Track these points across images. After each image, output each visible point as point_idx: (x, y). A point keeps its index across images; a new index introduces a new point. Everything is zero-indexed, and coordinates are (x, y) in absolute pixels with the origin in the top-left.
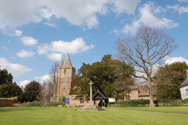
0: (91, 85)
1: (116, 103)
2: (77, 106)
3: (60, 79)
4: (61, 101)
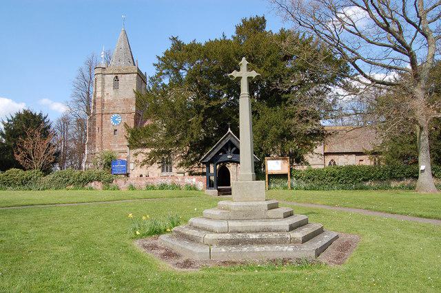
1: (291, 176)
2: (153, 188)
3: (103, 105)
4: (101, 170)
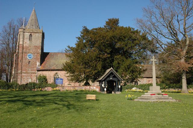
0: (154, 62)
3: (23, 48)
